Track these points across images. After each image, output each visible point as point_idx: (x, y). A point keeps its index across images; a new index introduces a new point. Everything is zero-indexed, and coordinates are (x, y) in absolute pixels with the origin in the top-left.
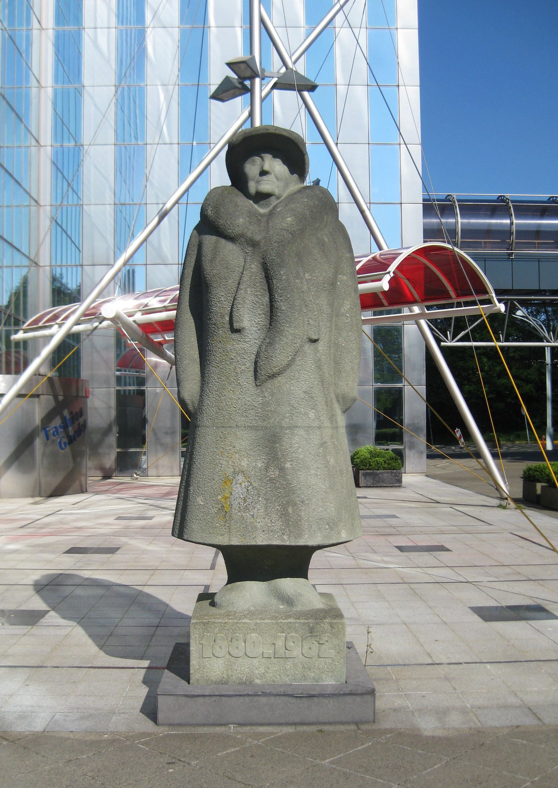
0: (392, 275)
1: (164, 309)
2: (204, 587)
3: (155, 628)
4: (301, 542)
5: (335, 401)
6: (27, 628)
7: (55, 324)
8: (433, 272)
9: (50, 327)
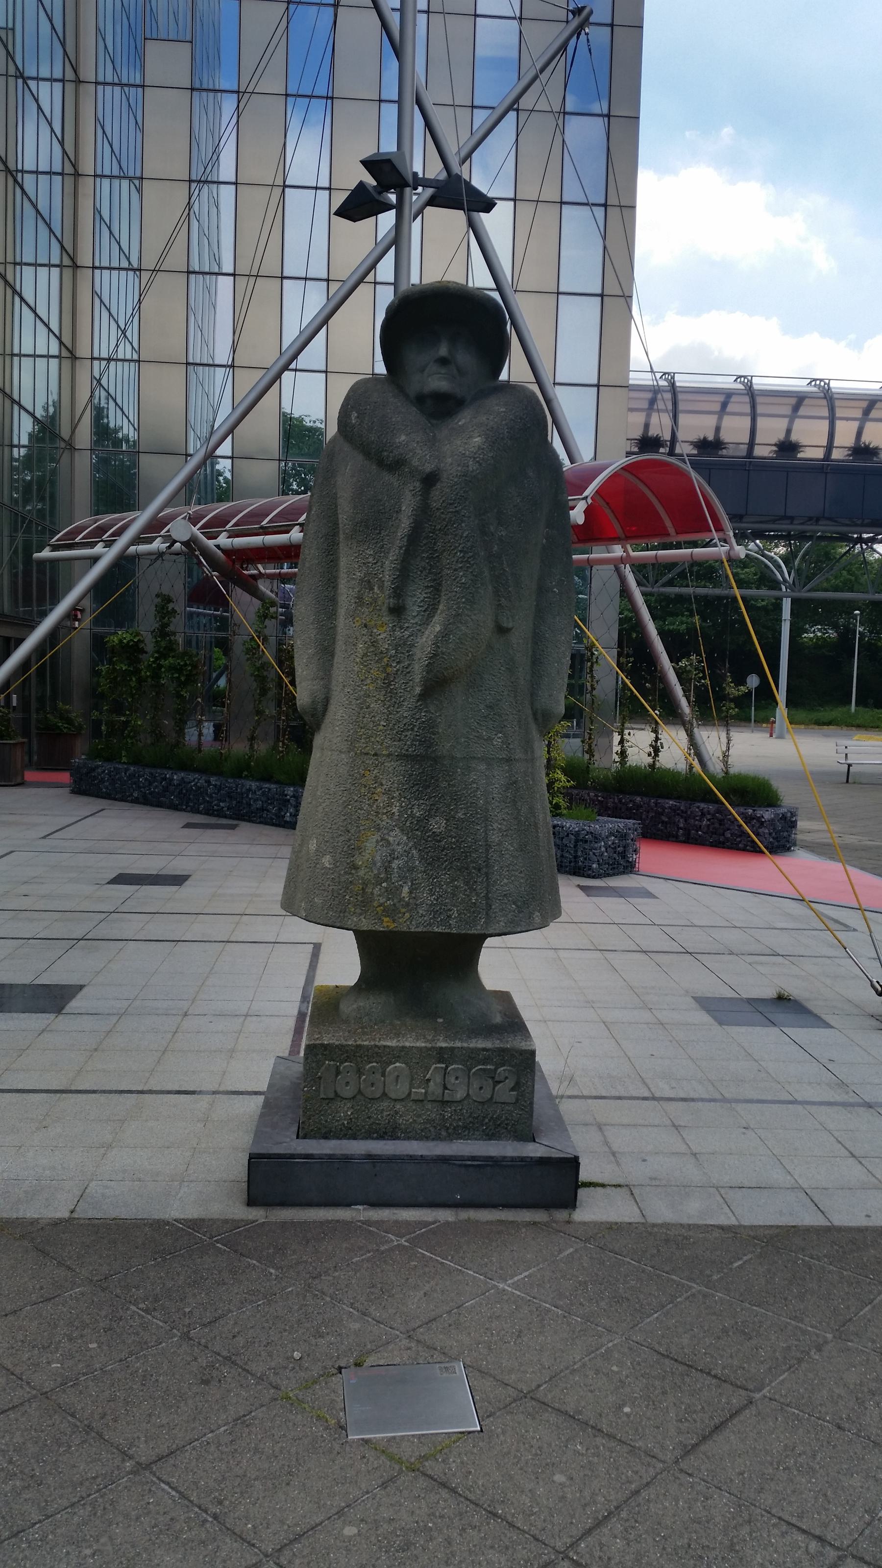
0: (590, 501)
1: (261, 530)
2: (312, 946)
3: (242, 1019)
4: (473, 931)
5: (530, 719)
6: (48, 1019)
7: (99, 541)
8: (650, 501)
9: (92, 545)
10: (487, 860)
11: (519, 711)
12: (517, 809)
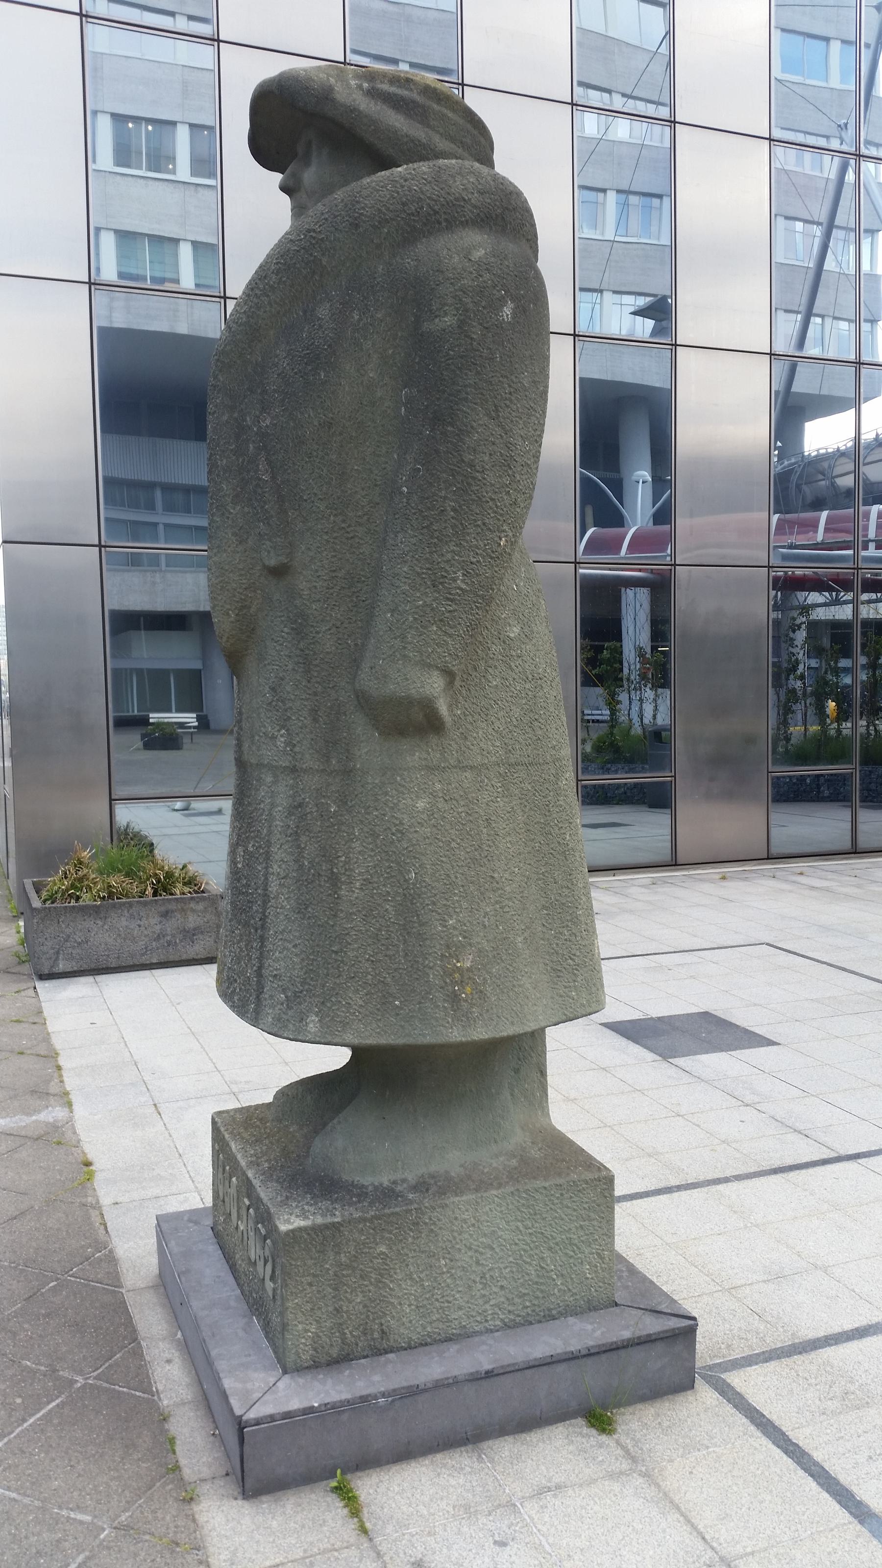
10: (264, 919)
11: (315, 694)
12: (299, 847)
